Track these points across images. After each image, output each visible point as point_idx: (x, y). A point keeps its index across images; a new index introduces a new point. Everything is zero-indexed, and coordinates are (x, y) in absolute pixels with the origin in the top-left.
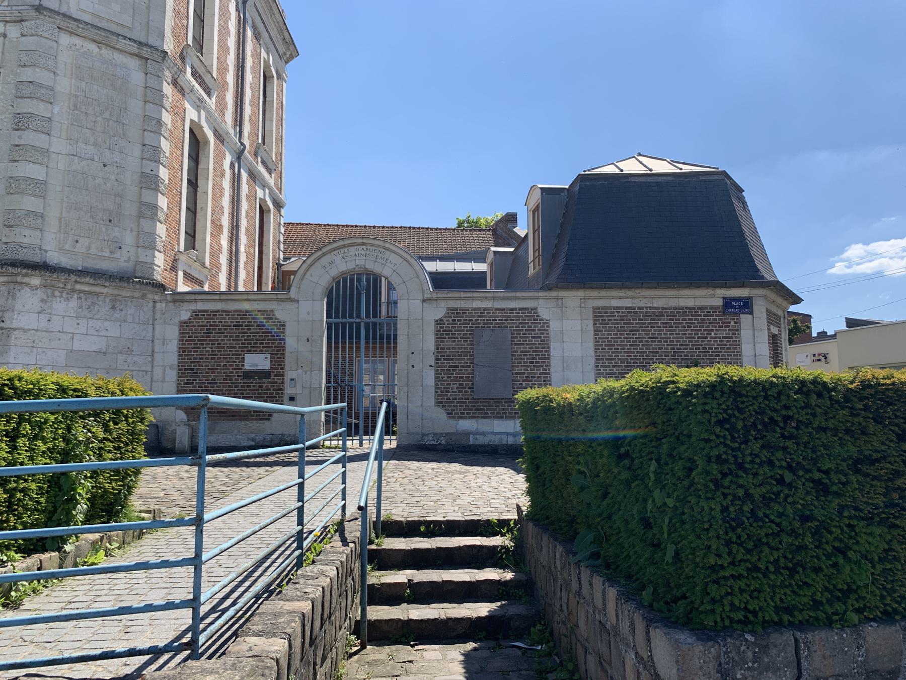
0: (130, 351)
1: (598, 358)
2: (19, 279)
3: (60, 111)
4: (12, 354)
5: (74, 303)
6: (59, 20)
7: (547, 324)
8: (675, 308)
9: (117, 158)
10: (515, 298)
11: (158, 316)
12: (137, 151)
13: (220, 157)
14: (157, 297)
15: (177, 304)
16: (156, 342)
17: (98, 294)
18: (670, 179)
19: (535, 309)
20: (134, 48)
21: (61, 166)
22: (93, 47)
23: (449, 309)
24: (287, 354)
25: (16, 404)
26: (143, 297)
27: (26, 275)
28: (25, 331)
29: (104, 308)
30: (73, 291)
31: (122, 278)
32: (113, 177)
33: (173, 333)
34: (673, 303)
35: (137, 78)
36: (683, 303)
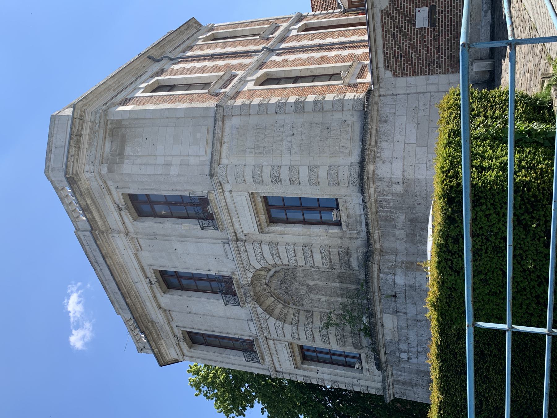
0: (416, 109)
2: (370, 176)
3: (265, 161)
5: (384, 145)
6: (215, 165)
11: (390, 93)
12: (281, 117)
15: (381, 81)
16: (408, 92)
17: (377, 132)
20: (219, 124)
22: (225, 147)
26: (377, 103)
27: (368, 173)
29: (386, 127)
30: (376, 146)
31: (365, 118)
32: (300, 129)
33: (402, 81)
35: (236, 121)
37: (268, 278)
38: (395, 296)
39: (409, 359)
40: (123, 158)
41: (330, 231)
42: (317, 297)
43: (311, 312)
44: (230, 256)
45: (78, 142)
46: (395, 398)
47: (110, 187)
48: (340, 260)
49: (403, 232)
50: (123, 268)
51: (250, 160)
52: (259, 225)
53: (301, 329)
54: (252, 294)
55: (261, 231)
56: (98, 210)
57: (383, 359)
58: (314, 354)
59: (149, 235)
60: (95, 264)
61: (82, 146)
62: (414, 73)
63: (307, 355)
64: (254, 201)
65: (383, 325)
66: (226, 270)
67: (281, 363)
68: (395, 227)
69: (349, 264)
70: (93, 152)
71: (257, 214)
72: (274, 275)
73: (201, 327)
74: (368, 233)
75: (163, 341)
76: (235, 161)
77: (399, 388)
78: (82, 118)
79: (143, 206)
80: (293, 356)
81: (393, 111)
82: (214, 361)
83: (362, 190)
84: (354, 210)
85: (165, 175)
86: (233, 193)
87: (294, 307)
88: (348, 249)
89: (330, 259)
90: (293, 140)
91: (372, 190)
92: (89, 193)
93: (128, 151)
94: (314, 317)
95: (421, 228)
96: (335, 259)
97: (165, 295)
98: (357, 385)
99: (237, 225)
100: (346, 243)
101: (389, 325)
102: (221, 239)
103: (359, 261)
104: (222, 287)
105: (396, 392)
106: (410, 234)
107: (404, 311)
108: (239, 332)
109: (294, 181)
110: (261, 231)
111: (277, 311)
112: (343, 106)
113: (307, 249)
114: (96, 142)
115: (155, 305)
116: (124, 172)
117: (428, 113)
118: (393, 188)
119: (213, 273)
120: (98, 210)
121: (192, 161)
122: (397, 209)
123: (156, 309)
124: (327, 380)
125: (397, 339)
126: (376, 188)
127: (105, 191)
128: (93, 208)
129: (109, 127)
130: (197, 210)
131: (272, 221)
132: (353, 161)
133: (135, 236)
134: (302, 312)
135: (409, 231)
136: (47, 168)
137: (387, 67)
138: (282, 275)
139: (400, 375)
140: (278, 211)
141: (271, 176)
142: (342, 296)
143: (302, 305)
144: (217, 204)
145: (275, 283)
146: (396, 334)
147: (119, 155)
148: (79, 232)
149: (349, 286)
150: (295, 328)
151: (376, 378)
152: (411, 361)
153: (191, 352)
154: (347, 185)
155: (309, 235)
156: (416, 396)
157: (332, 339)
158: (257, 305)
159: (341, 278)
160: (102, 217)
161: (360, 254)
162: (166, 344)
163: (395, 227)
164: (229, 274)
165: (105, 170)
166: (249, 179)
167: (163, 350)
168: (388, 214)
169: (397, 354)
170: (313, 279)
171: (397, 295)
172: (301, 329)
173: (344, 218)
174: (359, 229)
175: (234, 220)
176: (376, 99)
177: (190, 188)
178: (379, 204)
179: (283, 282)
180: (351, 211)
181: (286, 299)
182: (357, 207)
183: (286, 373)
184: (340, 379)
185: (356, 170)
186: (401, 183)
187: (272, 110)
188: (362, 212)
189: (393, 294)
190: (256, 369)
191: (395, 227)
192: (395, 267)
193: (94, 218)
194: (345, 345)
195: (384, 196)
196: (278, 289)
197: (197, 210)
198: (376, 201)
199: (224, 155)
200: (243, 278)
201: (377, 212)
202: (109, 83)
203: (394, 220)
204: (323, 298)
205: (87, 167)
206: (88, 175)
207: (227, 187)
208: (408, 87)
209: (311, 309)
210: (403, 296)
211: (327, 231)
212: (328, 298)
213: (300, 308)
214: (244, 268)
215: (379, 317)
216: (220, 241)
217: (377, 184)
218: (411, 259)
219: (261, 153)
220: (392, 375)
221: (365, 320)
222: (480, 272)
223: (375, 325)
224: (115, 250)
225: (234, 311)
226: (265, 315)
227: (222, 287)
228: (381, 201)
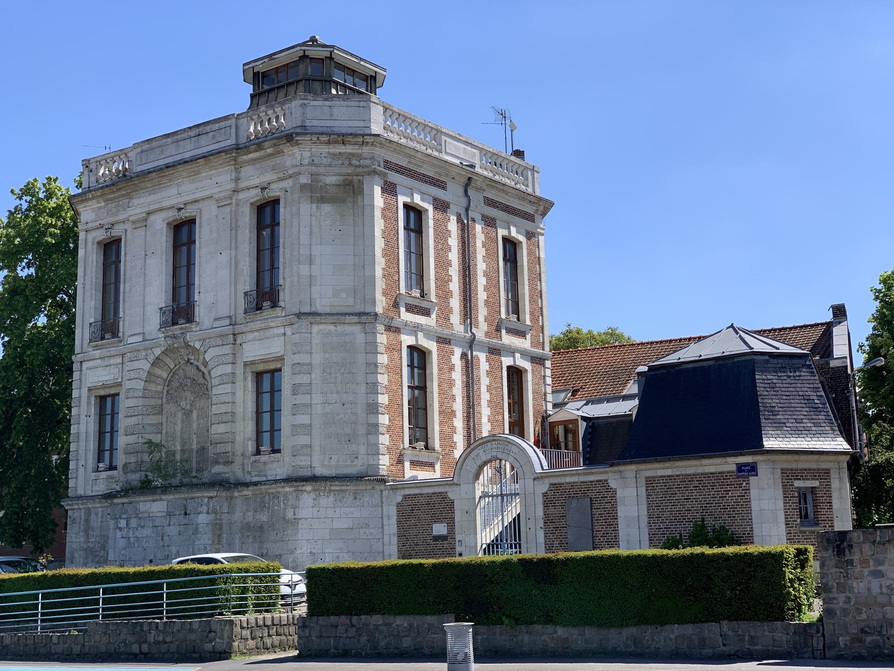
0: (367, 526)
1: (650, 516)
2: (300, 488)
3: (316, 375)
4: (300, 534)
5: (331, 498)
6: (310, 318)
7: (615, 492)
8: (702, 474)
9: (351, 398)
10: (592, 474)
11: (384, 500)
12: (363, 388)
13: (445, 358)
17: (345, 491)
18: (712, 363)
19: (607, 481)
20: (355, 319)
21: (319, 412)
23: (551, 484)
24: (456, 523)
25: (429, 556)
26: (373, 488)
27: (303, 486)
28: (306, 519)
29: (350, 499)
30: (330, 490)
31: (358, 478)
32: (349, 411)
33: (392, 512)
34: (700, 470)
35: (360, 338)
36: (708, 470)
37: (196, 363)
39: (120, 529)
40: (318, 202)
41: (250, 443)
42: (179, 421)
44: (217, 324)
45: (336, 142)
46: (67, 511)
51: (317, 358)
52: (252, 363)
53: (140, 402)
54: (176, 345)
55: (246, 365)
57: (116, 501)
58: (109, 411)
59: (236, 221)
60: (196, 131)
61: (331, 146)
63: (106, 403)
64: (276, 360)
65: (154, 501)
67: (93, 371)
69: (217, 462)
70: (324, 161)
71: (264, 361)
72: (200, 370)
73: (128, 268)
74: (247, 485)
75: (103, 204)
76: (316, 340)
79: (267, 213)
80: (104, 386)
82: (84, 276)
83: (288, 480)
87: (165, 393)
88: (232, 462)
91: (287, 489)
92: (279, 152)
93: (327, 208)
94: (155, 417)
96: (220, 448)
97: (165, 225)
98: (77, 465)
99: (251, 336)
100: (238, 460)
101: (155, 507)
102: (235, 315)
103: (220, 474)
104: (181, 310)
105: (75, 512)
107: (172, 523)
108: (127, 318)
109: (296, 408)
110: (246, 365)
111: (158, 371)
112: (373, 454)
113: (229, 417)
114: (337, 162)
115: (152, 208)
116: (302, 206)
119: (196, 298)
121: (316, 290)
123: (147, 209)
124: (78, 428)
125: (140, 515)
126: (290, 493)
127: (281, 175)
128: (262, 153)
129: (355, 178)
130: (265, 295)
131: (259, 376)
133: (234, 201)
134: (159, 402)
135: (252, 525)
137: (405, 497)
138: (201, 381)
139: (97, 516)
140: (267, 380)
141: (300, 385)
142: (183, 451)
143: (168, 402)
144: (271, 317)
145: (191, 371)
146: (146, 515)
147: (322, 197)
148: (234, 120)
149: (194, 460)
150: (141, 394)
151: (89, 487)
152: (118, 531)
153: (93, 244)
155: (244, 420)
156: (73, 536)
157: (132, 439)
158: (163, 349)
159: (202, 450)
162: (100, 208)
163: (256, 511)
164: (197, 319)
165: (304, 179)
166: (297, 359)
167: (90, 203)
169: (124, 516)
172: (140, 402)
173: (263, 458)
175: (256, 334)
176: (377, 487)
177: (287, 285)
178: (276, 496)
180: (270, 466)
182: (274, 473)
183: (81, 374)
184: (82, 443)
187: (370, 378)
188: (270, 478)
189: (188, 512)
190: (82, 334)
191: (256, 511)
192: (215, 513)
193: (250, 153)
194: (126, 453)
196: (184, 378)
197: (265, 295)
198: (279, 493)
199: (322, 327)
200: (194, 336)
201: (269, 494)
202: (419, 155)
203: (262, 510)
204: (178, 428)
205: (307, 154)
206: (298, 155)
207: (289, 331)
209: (164, 412)
211: (249, 439)
212: (178, 434)
213: (164, 400)
214: (204, 340)
215: (163, 498)
216: (232, 313)
218: (225, 527)
220: (96, 508)
223: (154, 493)
225: (154, 321)
226: (152, 358)
227: (181, 310)
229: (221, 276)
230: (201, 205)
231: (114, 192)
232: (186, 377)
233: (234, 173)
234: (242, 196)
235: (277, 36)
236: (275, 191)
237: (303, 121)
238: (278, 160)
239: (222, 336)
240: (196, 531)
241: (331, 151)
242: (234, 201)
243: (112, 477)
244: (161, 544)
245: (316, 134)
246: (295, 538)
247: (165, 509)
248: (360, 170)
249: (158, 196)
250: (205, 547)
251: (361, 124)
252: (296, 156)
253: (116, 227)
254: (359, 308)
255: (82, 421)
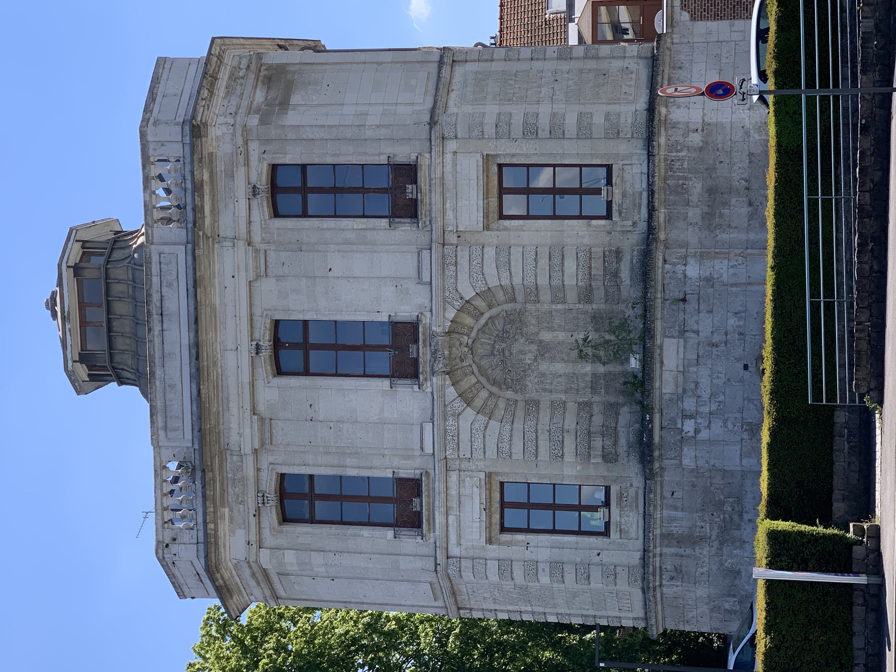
0: (718, 56)
14: (669, 41)
15: (675, 24)
16: (709, 40)
17: (660, 567)
20: (446, 70)
22: (453, 95)
28: (704, 115)
32: (566, 76)
33: (702, 26)
38: (684, 300)
43: (537, 403)
45: (212, 84)
47: (252, 152)
48: (605, 267)
49: (698, 211)
50: (215, 316)
53: (518, 425)
56: (213, 196)
62: (717, 17)
64: (488, 171)
66: (408, 308)
68: (688, 205)
75: (226, 510)
76: (469, 109)
77: (672, 555)
78: (220, 57)
81: (690, 58)
84: (632, 185)
85: (358, 126)
86: (459, 156)
89: (590, 268)
90: (556, 86)
91: (662, 140)
92: (211, 161)
93: (295, 99)
94: (541, 411)
95: (722, 203)
96: (598, 268)
99: (450, 215)
104: (397, 351)
106: (707, 213)
107: (695, 327)
115: (247, 405)
117: (732, 60)
118: (690, 139)
120: (213, 196)
122: (692, 173)
123: (248, 414)
125: (680, 390)
127: (241, 159)
128: (207, 189)
132: (638, 108)
135: (706, 209)
136: (145, 122)
143: (523, 390)
146: (680, 378)
154: (629, 136)
160: (215, 211)
161: (635, 253)
162: (231, 519)
163: (687, 203)
168: (681, 182)
170: (551, 329)
171: (688, 297)
174: (636, 218)
175: (448, 205)
179: (503, 336)
181: (498, 378)
185: (643, 117)
186: (700, 130)
189: (682, 297)
191: (687, 203)
193: (203, 207)
195: (677, 151)
198: (666, 160)
199: (451, 103)
200: (436, 323)
201: (666, 179)
204: (560, 367)
208: (709, 33)
210: (696, 296)
215: (658, 342)
217: (670, 133)
219: (509, 100)
221: (634, 363)
222: (812, 587)
224: (214, 277)
226: (459, 405)
227: (397, 351)
228: (672, 161)
229: (363, 274)
230: (258, 311)
231: (215, 482)
232: (492, 354)
233: (225, 244)
234: (257, 238)
235: (45, 344)
236: (260, 174)
237: (177, 124)
238: (220, 166)
239: (443, 266)
240: (709, 281)
241: (222, 94)
242: (263, 247)
243: (620, 497)
244: (722, 348)
245: (197, 99)
246: (728, 128)
247: (675, 341)
248: (253, 67)
249: (233, 392)
250: (732, 267)
251: (193, 68)
252: (220, 137)
253: (263, 487)
254: (434, 68)
255: (534, 557)
